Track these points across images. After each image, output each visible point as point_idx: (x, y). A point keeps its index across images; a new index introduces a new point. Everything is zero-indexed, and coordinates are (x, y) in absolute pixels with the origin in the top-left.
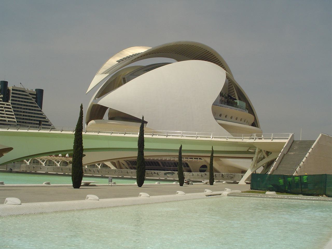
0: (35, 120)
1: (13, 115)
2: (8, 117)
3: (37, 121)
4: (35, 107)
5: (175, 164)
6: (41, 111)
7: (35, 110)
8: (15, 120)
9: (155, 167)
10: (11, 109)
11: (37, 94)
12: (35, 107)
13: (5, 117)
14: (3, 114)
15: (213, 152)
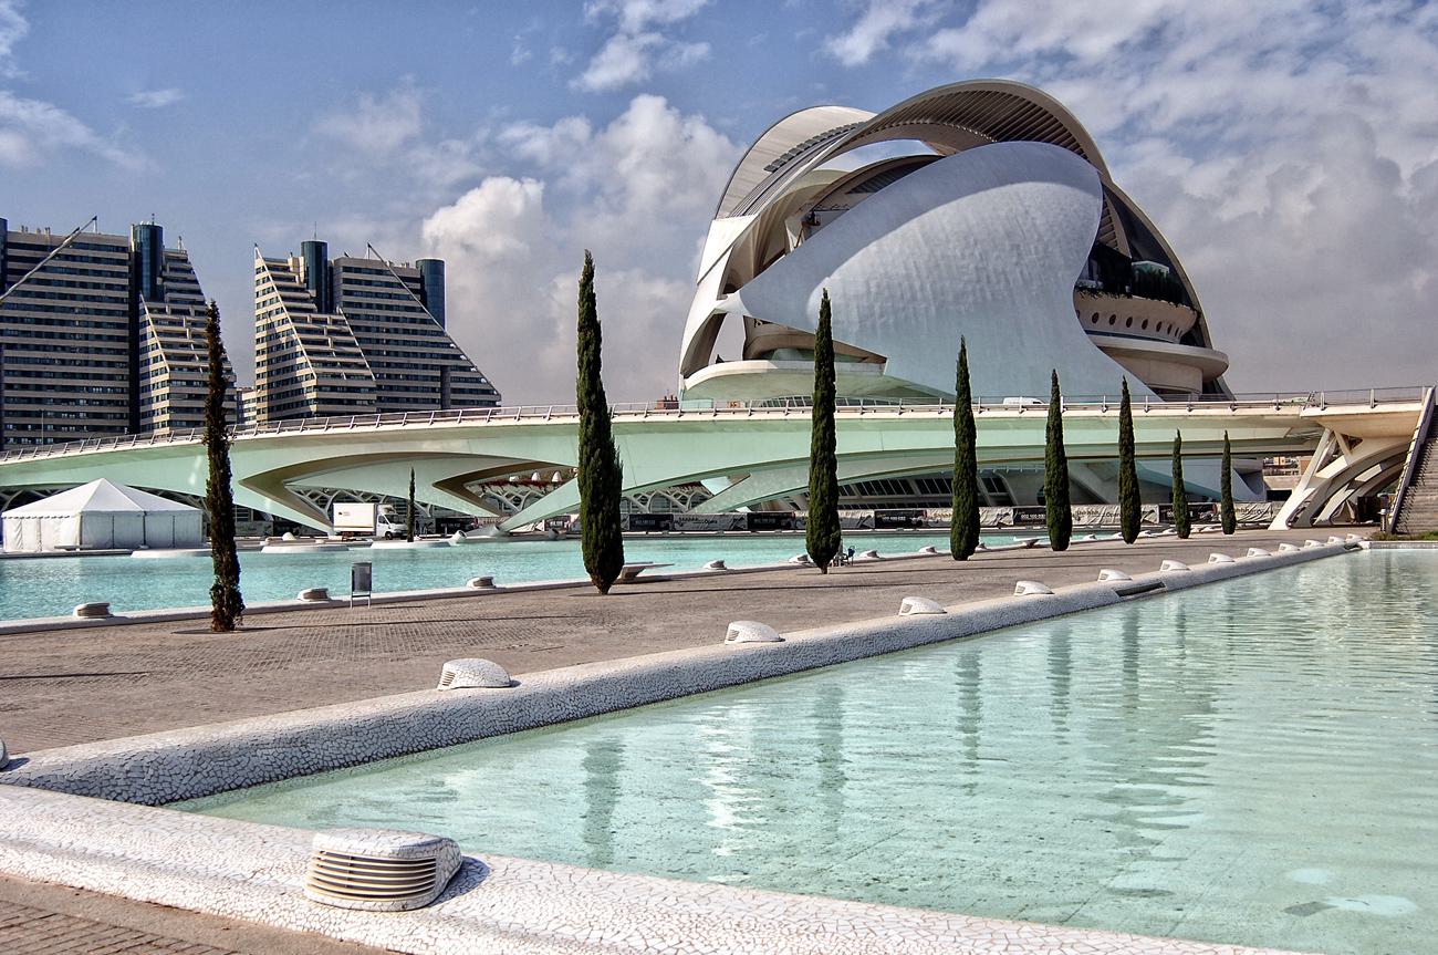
0: (425, 367)
1: (358, 355)
2: (344, 365)
3: (433, 367)
4: (424, 321)
5: (931, 487)
6: (441, 334)
7: (425, 333)
8: (369, 372)
9: (887, 496)
10: (348, 334)
11: (422, 277)
12: (424, 321)
13: (334, 364)
14: (328, 353)
15: (1227, 443)
